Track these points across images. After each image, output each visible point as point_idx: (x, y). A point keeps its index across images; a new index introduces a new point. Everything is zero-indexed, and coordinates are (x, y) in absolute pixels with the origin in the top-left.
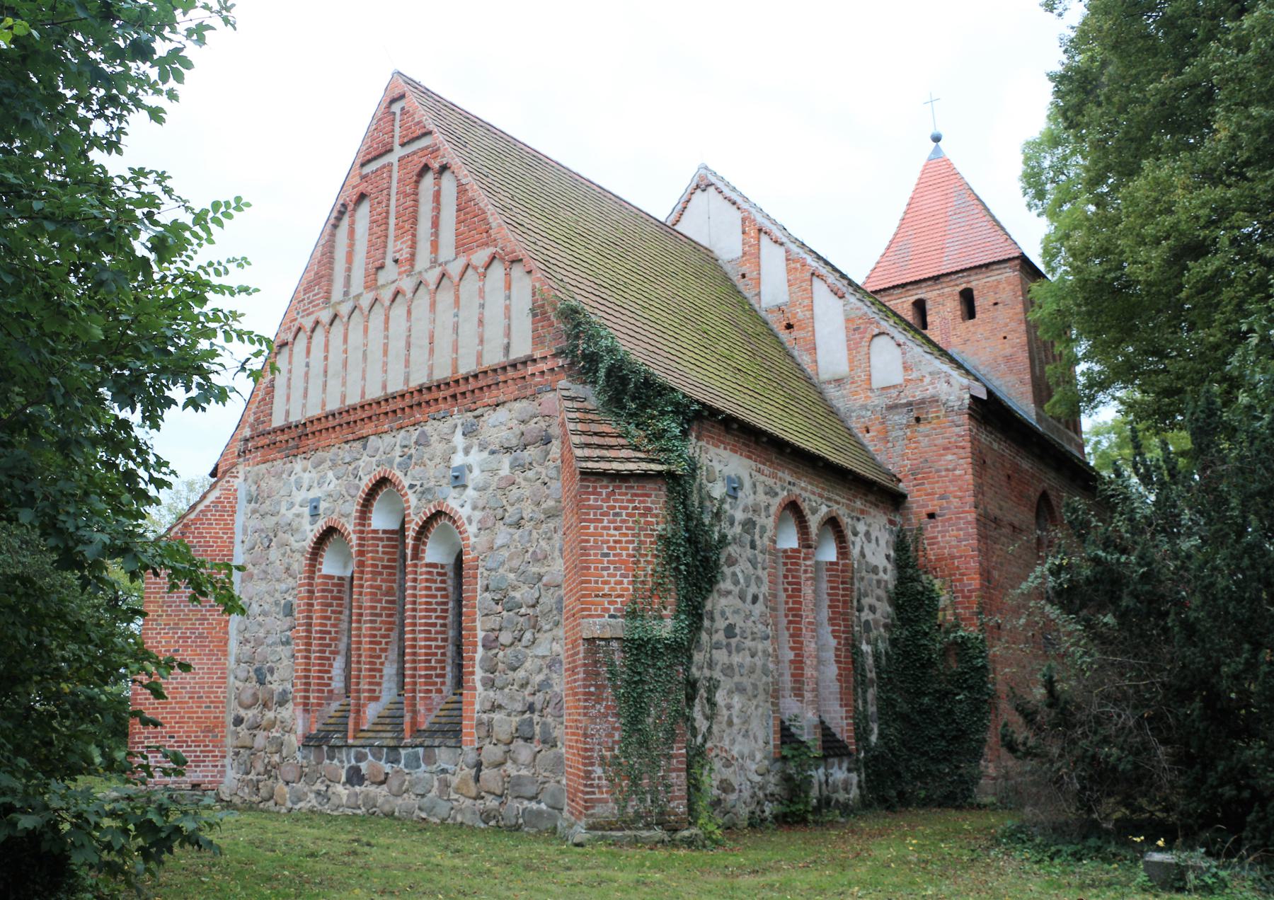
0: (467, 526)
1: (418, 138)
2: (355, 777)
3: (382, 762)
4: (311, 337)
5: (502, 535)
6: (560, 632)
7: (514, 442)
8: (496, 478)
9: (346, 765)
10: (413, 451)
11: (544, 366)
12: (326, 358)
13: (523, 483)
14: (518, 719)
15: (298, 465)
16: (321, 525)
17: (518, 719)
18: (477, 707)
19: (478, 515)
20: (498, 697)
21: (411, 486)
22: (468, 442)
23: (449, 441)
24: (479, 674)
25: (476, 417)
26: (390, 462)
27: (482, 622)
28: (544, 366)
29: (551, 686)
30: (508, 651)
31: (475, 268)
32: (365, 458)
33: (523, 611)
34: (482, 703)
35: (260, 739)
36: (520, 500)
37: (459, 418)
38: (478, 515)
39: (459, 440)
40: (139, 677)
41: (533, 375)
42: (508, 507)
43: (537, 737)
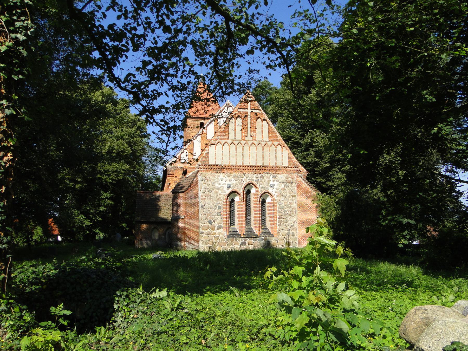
1: (256, 110)
5: (282, 198)
6: (296, 217)
12: (229, 152)
15: (222, 175)
16: (231, 190)
19: (276, 194)
24: (278, 224)
28: (292, 169)
31: (274, 145)
35: (211, 236)
37: (271, 175)
39: (271, 178)
40: (219, 57)
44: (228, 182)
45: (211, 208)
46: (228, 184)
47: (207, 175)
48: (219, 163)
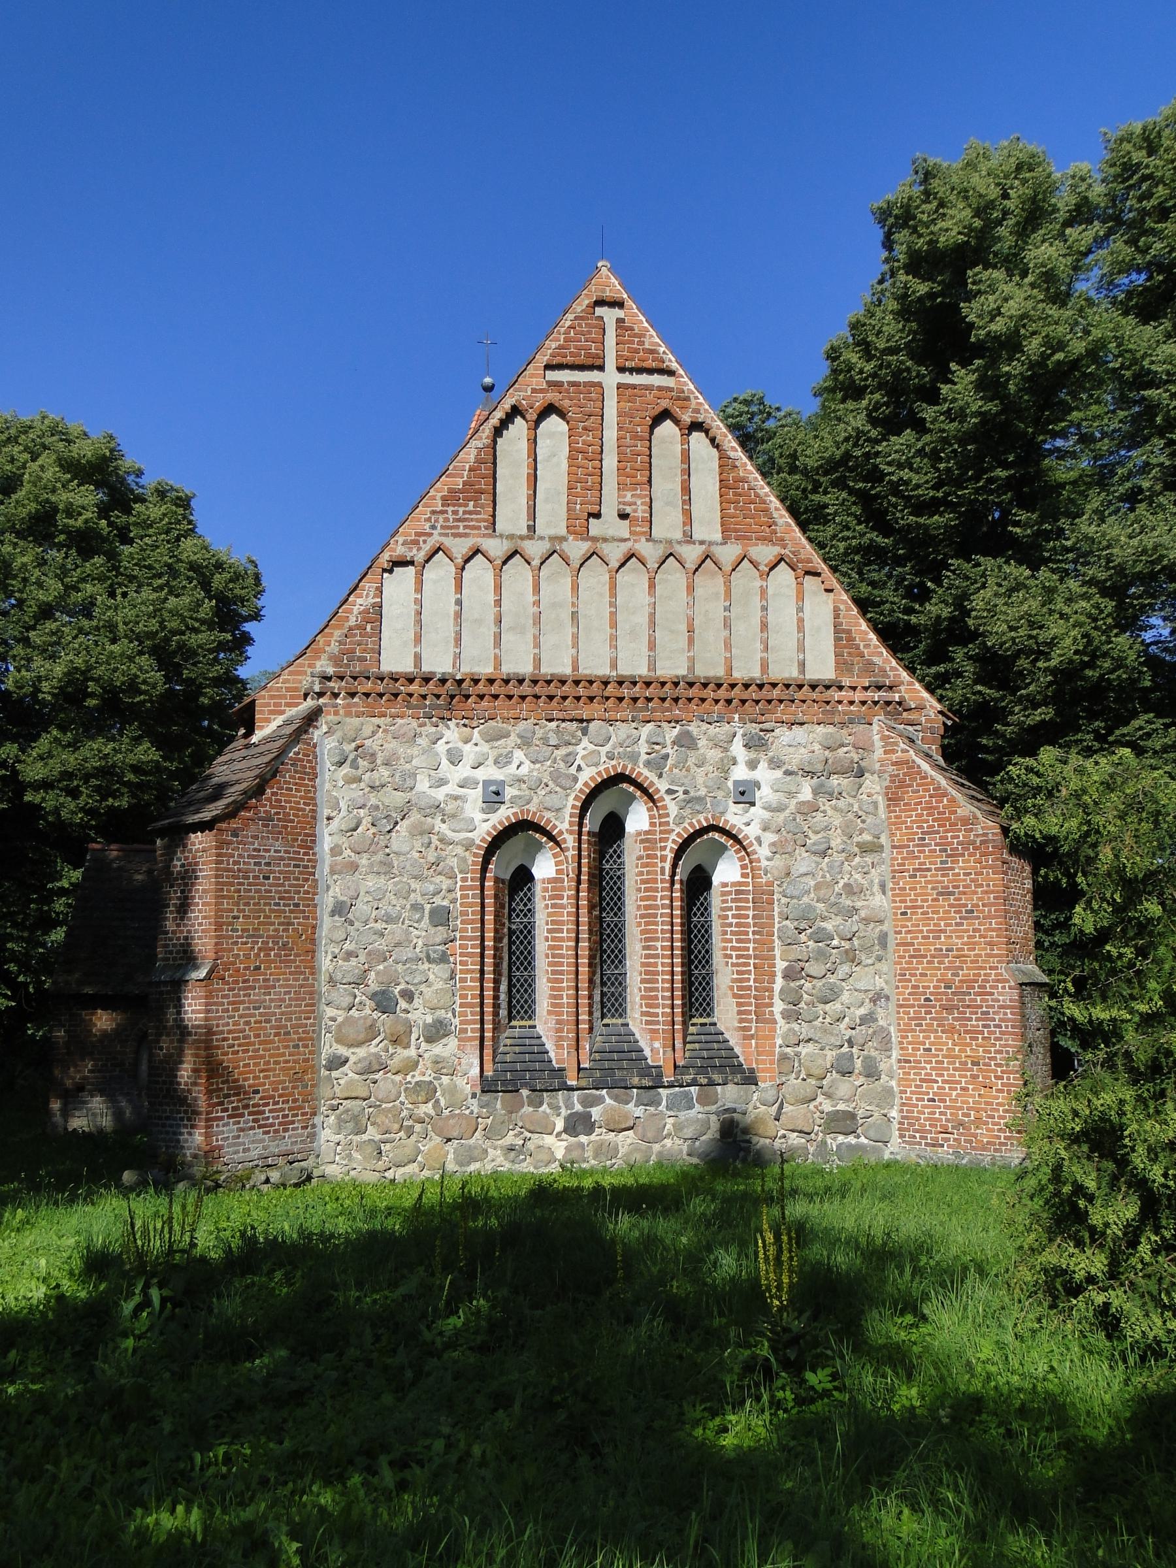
0: (756, 846)
1: (650, 371)
2: (578, 1124)
3: (631, 1105)
4: (463, 569)
5: (803, 862)
6: (884, 967)
7: (820, 767)
8: (794, 801)
9: (564, 1112)
10: (668, 750)
11: (858, 696)
12: (498, 603)
13: (830, 812)
14: (834, 1053)
15: (452, 733)
16: (504, 815)
17: (834, 1053)
18: (779, 1041)
19: (770, 837)
20: (804, 1030)
21: (670, 792)
22: (753, 755)
23: (726, 750)
25: (762, 730)
26: (634, 757)
27: (783, 952)
29: (876, 1020)
30: (819, 984)
32: (585, 742)
33: (835, 943)
34: (784, 1037)
36: (827, 828)
38: (770, 837)
39: (738, 748)
41: (840, 702)
42: (811, 834)
43: (857, 1071)
44: (490, 772)
45: (389, 919)
46: (487, 783)
47: (367, 731)
48: (439, 663)
